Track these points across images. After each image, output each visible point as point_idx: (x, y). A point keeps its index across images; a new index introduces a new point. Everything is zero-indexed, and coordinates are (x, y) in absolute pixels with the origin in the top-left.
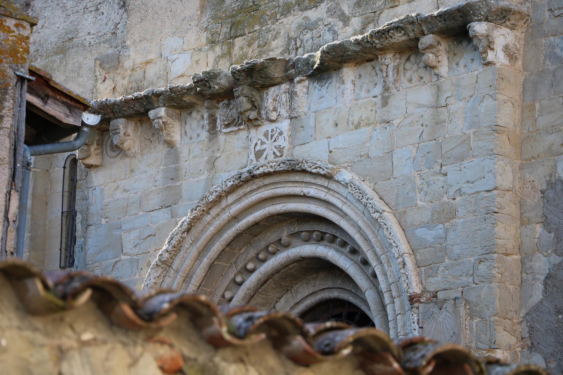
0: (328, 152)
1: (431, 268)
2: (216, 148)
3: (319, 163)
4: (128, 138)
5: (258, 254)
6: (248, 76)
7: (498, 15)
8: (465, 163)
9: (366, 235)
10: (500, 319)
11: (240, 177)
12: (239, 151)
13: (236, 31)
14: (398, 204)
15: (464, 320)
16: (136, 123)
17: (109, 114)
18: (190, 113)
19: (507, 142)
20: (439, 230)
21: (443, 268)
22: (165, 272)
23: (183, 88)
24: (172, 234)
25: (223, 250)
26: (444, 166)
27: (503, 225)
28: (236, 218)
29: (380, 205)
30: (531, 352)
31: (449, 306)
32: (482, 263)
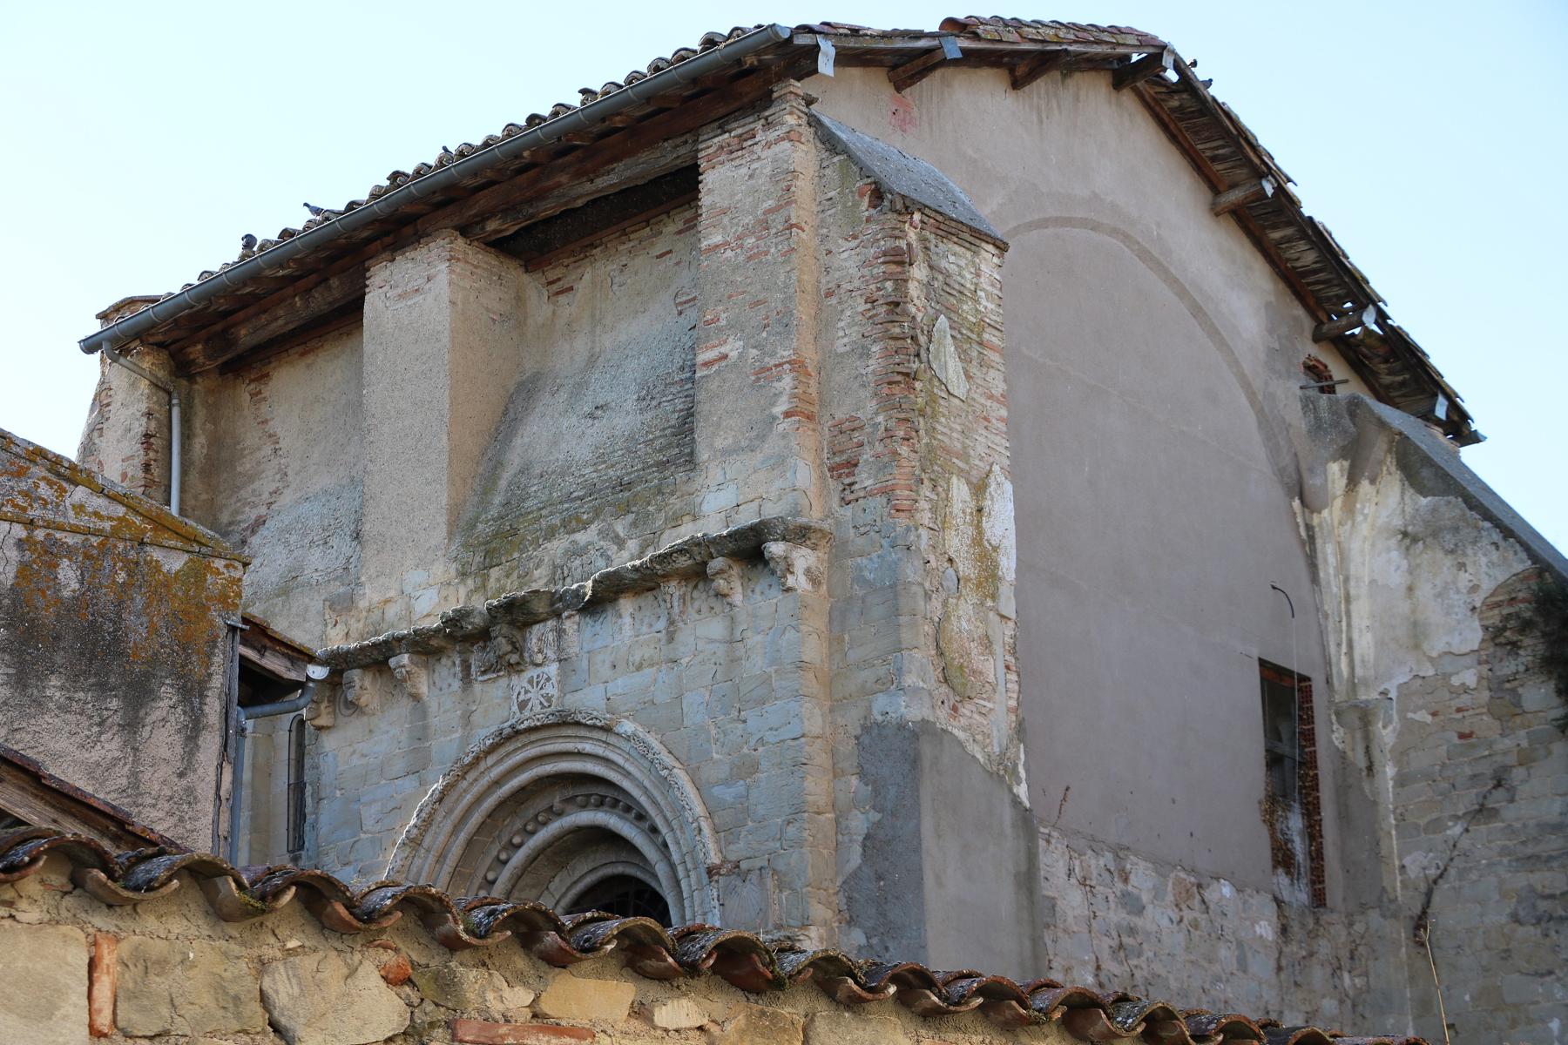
8: (767, 707)
12: (500, 701)
23: (429, 630)
28: (497, 783)
29: (669, 760)
31: (754, 877)
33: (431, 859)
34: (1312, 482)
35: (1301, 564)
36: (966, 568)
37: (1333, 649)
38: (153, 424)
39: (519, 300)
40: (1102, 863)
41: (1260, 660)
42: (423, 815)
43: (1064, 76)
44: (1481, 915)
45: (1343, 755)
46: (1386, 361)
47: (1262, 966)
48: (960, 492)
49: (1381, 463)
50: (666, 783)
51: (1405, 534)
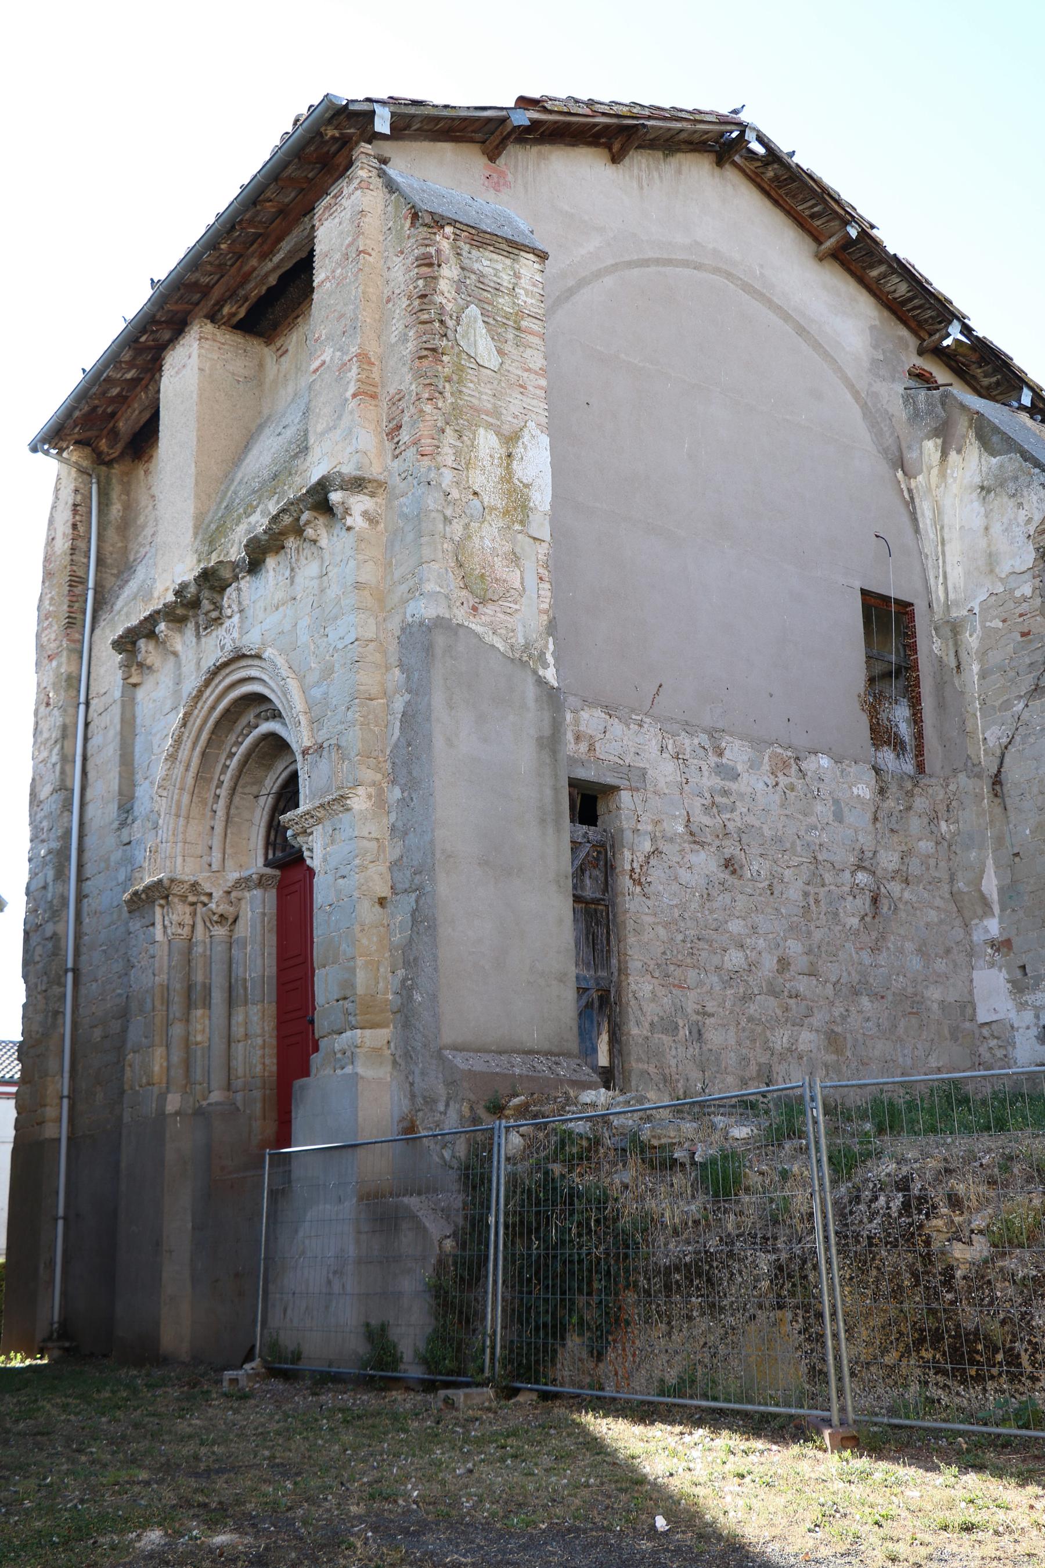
7: (352, 484)
8: (339, 622)
12: (215, 647)
25: (210, 738)
28: (213, 708)
33: (182, 769)
34: (911, 456)
35: (906, 519)
36: (492, 497)
37: (932, 581)
39: (261, 366)
40: (696, 741)
41: (864, 593)
43: (666, 156)
44: (1037, 769)
45: (940, 660)
46: (981, 367)
47: (859, 819)
48: (487, 442)
49: (964, 437)
51: (982, 488)
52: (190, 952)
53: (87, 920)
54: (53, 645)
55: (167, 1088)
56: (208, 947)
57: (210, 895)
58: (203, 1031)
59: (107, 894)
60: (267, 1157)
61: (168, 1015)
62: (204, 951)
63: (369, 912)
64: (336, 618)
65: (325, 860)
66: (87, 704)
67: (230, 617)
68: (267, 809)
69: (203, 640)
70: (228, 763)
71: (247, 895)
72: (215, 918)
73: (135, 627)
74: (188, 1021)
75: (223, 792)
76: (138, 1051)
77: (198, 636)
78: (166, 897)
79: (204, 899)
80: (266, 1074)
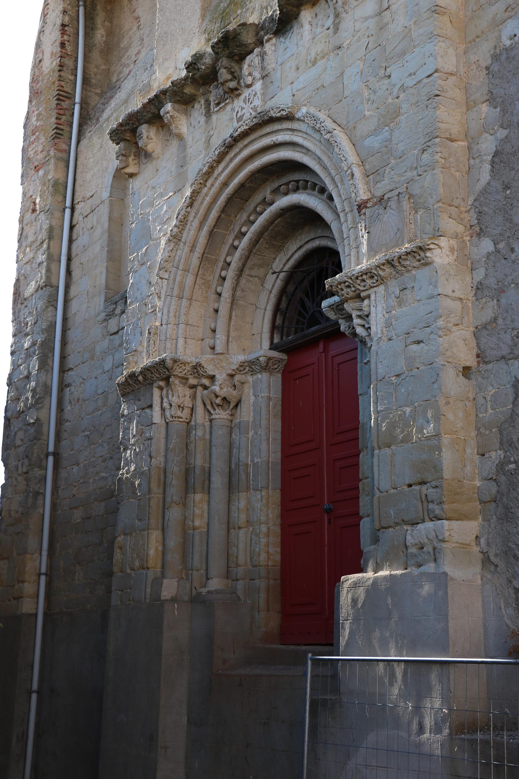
0: (292, 97)
1: (379, 174)
2: (210, 128)
3: (282, 106)
4: (151, 141)
5: (249, 217)
6: (224, 48)
8: (408, 57)
9: (325, 164)
10: (444, 206)
11: (224, 144)
12: (227, 122)
13: (225, 22)
14: (348, 122)
15: (408, 214)
16: (158, 129)
17: (136, 123)
18: (193, 107)
19: (449, 25)
20: (385, 133)
21: (389, 170)
22: (177, 246)
23: (181, 79)
24: (179, 210)
25: (219, 217)
26: (388, 67)
27: (446, 109)
28: (225, 184)
29: (329, 124)
30: (480, 238)
31: (393, 204)
32: (425, 152)
33: (187, 249)
38: (67, 18)
42: (180, 217)
50: (330, 145)
52: (188, 436)
53: (69, 408)
54: (41, 156)
55: (162, 573)
56: (208, 430)
57: (212, 378)
58: (202, 516)
59: (90, 381)
60: (309, 662)
61: (164, 499)
62: (204, 435)
63: (452, 383)
64: (404, 53)
65: (388, 325)
66: (73, 209)
67: (249, 86)
68: (275, 291)
69: (214, 117)
70: (236, 243)
71: (250, 379)
72: (218, 401)
73: (138, 112)
74: (185, 505)
75: (231, 274)
76: (130, 534)
77: (208, 114)
78: (167, 379)
79: (206, 382)
80: (270, 563)
